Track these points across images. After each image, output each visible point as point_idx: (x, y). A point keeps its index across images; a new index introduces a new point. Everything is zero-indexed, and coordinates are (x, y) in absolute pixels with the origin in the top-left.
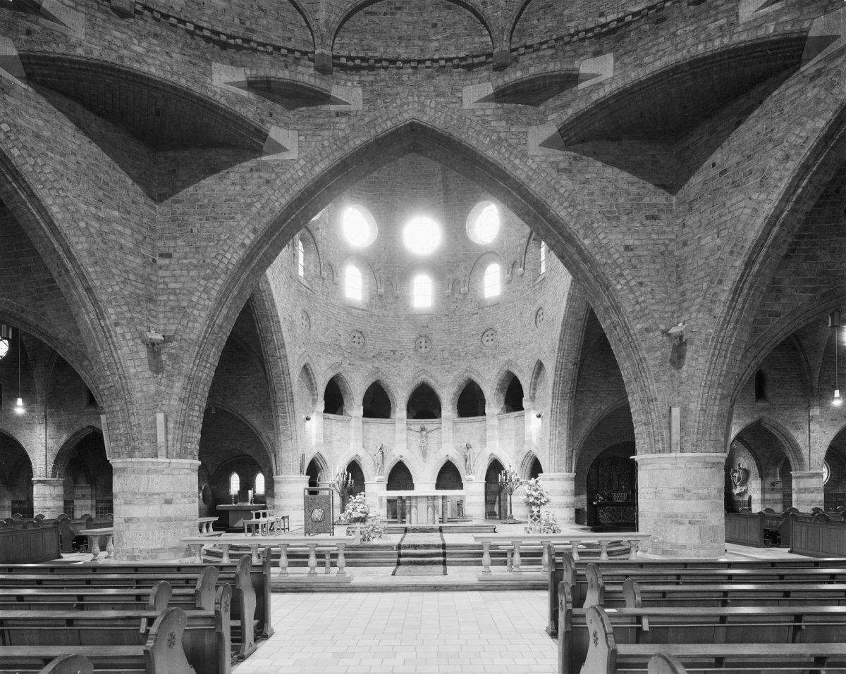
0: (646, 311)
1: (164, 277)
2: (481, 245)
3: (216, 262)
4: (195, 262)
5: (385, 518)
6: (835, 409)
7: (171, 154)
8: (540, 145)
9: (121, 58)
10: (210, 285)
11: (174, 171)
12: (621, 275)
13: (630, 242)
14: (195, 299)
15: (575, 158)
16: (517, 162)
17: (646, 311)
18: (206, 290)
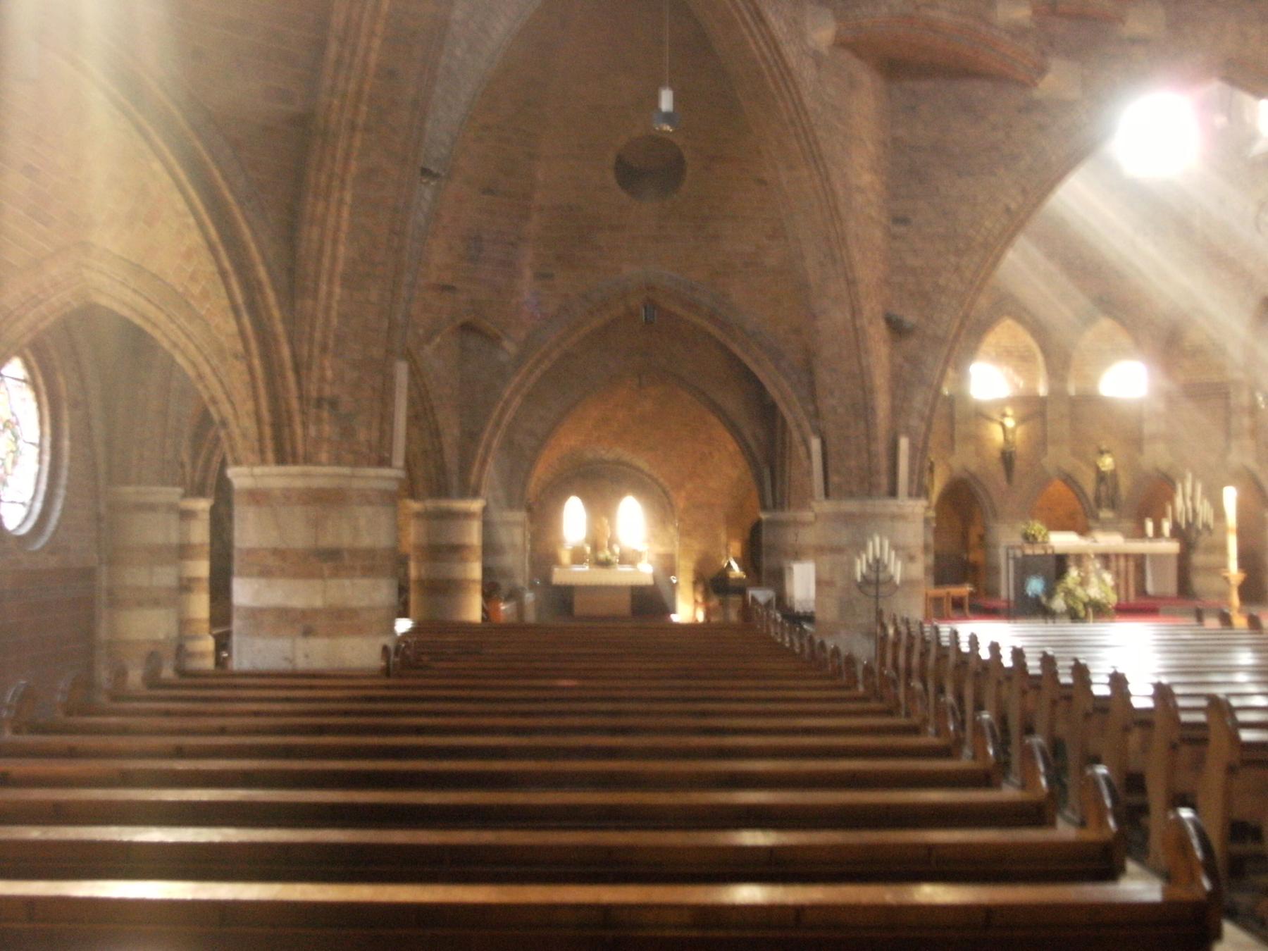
14: (942, 281)
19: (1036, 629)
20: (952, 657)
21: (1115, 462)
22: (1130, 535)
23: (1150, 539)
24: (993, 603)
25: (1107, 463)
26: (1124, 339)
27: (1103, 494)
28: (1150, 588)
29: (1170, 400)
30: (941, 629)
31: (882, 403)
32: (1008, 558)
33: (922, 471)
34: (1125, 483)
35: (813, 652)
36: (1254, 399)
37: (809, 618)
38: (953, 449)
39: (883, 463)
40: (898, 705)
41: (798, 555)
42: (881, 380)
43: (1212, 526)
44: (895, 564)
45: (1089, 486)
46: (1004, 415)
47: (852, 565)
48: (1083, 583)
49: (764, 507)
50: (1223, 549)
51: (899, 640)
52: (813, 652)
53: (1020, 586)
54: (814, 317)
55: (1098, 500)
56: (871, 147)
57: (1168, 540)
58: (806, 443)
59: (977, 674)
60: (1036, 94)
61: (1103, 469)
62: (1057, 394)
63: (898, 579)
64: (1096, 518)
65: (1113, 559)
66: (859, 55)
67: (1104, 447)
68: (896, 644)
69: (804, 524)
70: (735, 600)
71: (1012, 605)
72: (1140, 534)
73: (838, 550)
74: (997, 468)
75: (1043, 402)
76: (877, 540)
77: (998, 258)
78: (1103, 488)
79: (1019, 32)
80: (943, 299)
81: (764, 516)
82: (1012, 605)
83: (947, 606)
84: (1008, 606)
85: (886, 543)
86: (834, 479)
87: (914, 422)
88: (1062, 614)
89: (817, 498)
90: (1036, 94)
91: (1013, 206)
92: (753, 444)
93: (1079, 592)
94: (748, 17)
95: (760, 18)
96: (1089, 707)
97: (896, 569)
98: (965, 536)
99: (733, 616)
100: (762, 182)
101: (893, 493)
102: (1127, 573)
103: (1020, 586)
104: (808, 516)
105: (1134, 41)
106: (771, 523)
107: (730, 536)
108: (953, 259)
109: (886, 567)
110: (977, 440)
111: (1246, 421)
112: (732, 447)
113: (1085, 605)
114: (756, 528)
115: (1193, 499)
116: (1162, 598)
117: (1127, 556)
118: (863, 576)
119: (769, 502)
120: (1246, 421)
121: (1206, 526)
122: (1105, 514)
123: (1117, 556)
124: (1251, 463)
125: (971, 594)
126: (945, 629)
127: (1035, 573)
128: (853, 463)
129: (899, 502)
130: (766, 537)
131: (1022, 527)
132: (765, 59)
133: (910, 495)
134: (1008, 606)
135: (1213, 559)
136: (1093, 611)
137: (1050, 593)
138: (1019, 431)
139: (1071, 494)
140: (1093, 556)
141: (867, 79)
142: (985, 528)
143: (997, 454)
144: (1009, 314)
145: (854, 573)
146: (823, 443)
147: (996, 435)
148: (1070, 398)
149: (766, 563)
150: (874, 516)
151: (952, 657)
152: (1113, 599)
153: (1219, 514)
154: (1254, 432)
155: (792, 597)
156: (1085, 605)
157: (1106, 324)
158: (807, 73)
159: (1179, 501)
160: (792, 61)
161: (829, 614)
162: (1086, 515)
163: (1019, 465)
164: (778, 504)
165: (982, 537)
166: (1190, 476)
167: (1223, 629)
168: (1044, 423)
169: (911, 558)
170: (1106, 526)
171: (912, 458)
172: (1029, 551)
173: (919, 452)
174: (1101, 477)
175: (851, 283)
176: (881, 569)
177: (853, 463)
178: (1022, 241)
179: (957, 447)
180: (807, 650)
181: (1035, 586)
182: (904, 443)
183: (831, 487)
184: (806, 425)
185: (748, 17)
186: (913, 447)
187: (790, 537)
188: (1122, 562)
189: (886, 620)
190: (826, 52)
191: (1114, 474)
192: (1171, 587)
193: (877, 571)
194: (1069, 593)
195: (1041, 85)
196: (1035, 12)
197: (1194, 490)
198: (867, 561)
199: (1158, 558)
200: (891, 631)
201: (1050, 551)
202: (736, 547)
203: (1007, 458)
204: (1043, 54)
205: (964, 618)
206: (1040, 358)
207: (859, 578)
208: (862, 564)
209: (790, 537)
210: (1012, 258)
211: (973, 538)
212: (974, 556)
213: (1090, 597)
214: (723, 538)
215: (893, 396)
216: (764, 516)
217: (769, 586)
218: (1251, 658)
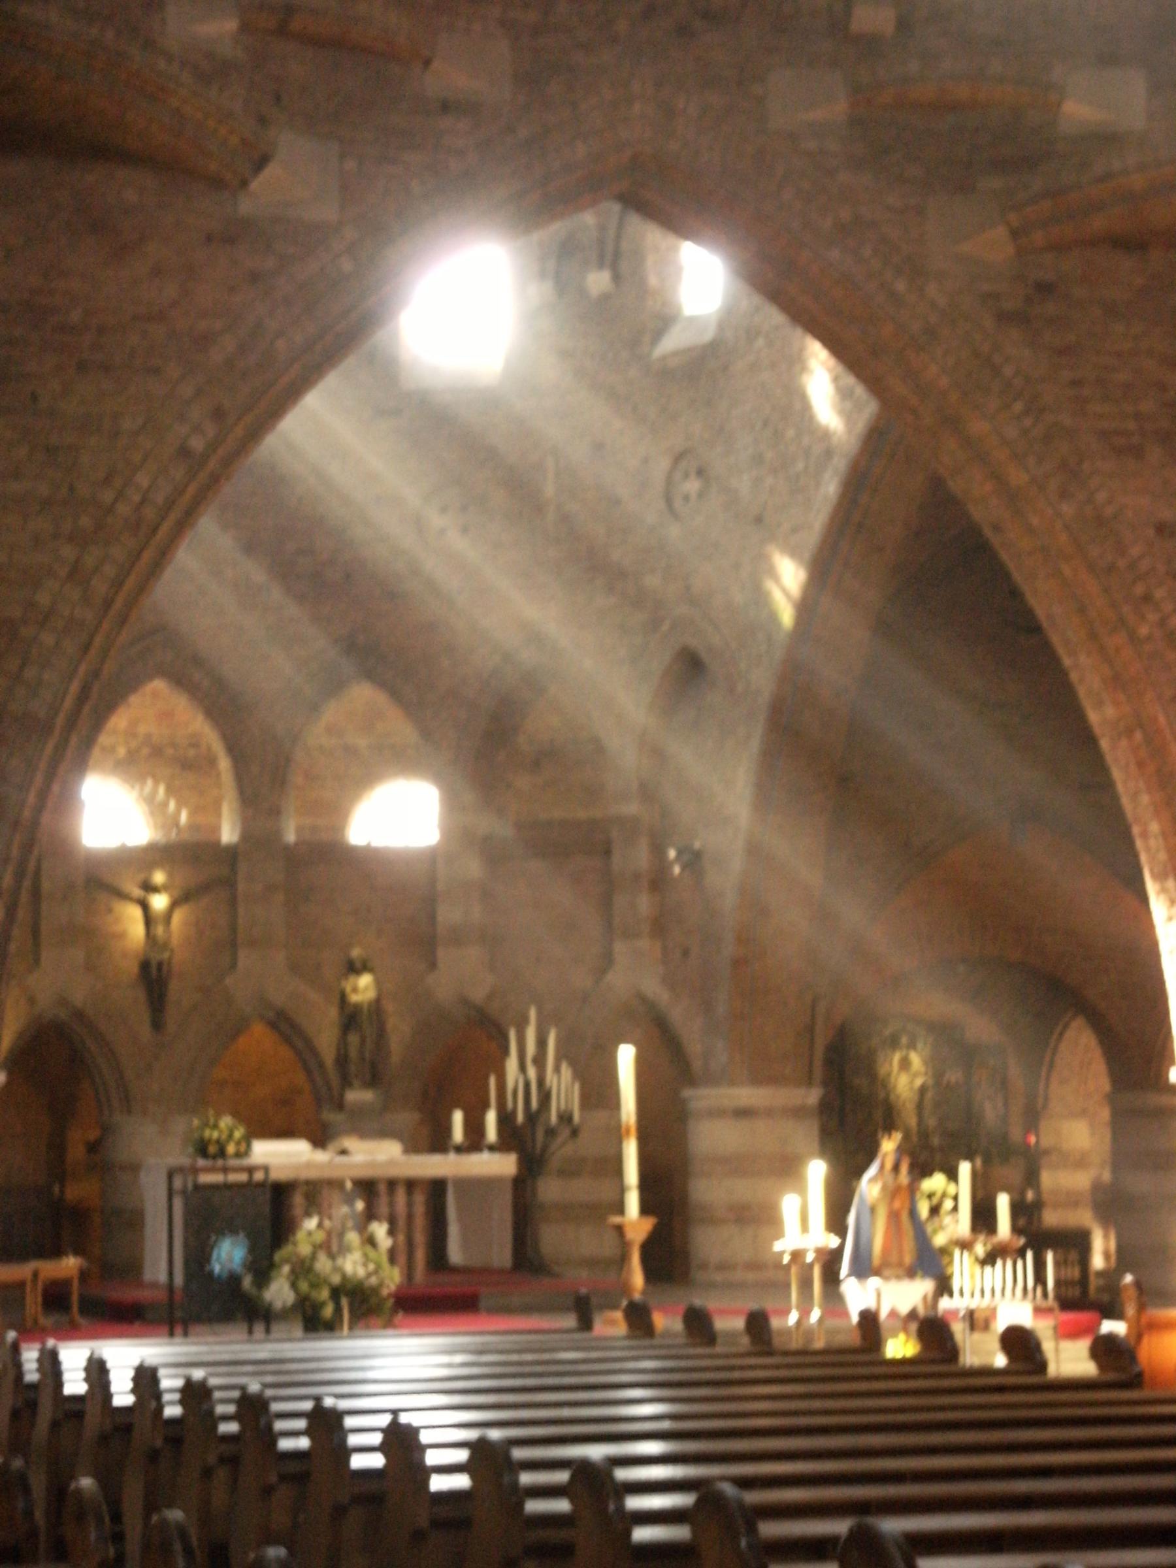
14: (43, 599)
19: (217, 1348)
20: (93, 1420)
21: (378, 982)
23: (459, 1149)
25: (363, 987)
26: (401, 728)
27: (353, 1053)
28: (455, 1254)
38: (37, 961)
40: (33, 1534)
45: (326, 1040)
46: (150, 888)
48: (332, 1246)
50: (618, 1170)
53: (198, 1257)
55: (342, 1060)
59: (153, 1456)
64: (340, 1106)
67: (356, 953)
72: (439, 1142)
74: (134, 1001)
75: (231, 855)
77: (164, 554)
78: (353, 1039)
80: (48, 639)
88: (285, 1315)
90: (245, 206)
91: (197, 444)
93: (323, 1264)
96: (423, 1522)
98: (58, 1147)
102: (410, 1217)
103: (198, 1257)
108: (68, 552)
111: (644, 903)
113: (336, 1293)
115: (539, 1060)
116: (483, 1272)
117: (411, 1184)
120: (644, 903)
121: (566, 1117)
122: (357, 1096)
123: (392, 1184)
124: (653, 987)
125: (84, 1275)
127: (230, 1228)
131: (181, 1125)
135: (581, 1190)
137: (262, 1270)
138: (177, 918)
139: (285, 1052)
140: (349, 1185)
142: (107, 1129)
143: (133, 968)
148: (286, 848)
151: (46, 1413)
152: (392, 1278)
154: (659, 927)
156: (336, 1293)
157: (363, 694)
162: (318, 1101)
163: (179, 993)
165: (93, 1147)
166: (533, 1014)
168: (233, 902)
172: (206, 1178)
174: (351, 1018)
178: (207, 525)
179: (48, 955)
188: (401, 1197)
191: (377, 1006)
192: (502, 1255)
194: (303, 1269)
195: (255, 185)
196: (245, 27)
197: (542, 1043)
201: (259, 1176)
204: (263, 120)
205: (72, 1332)
206: (224, 764)
211: (76, 1152)
212: (74, 1192)
213: (344, 1276)
218: (284, 1302)
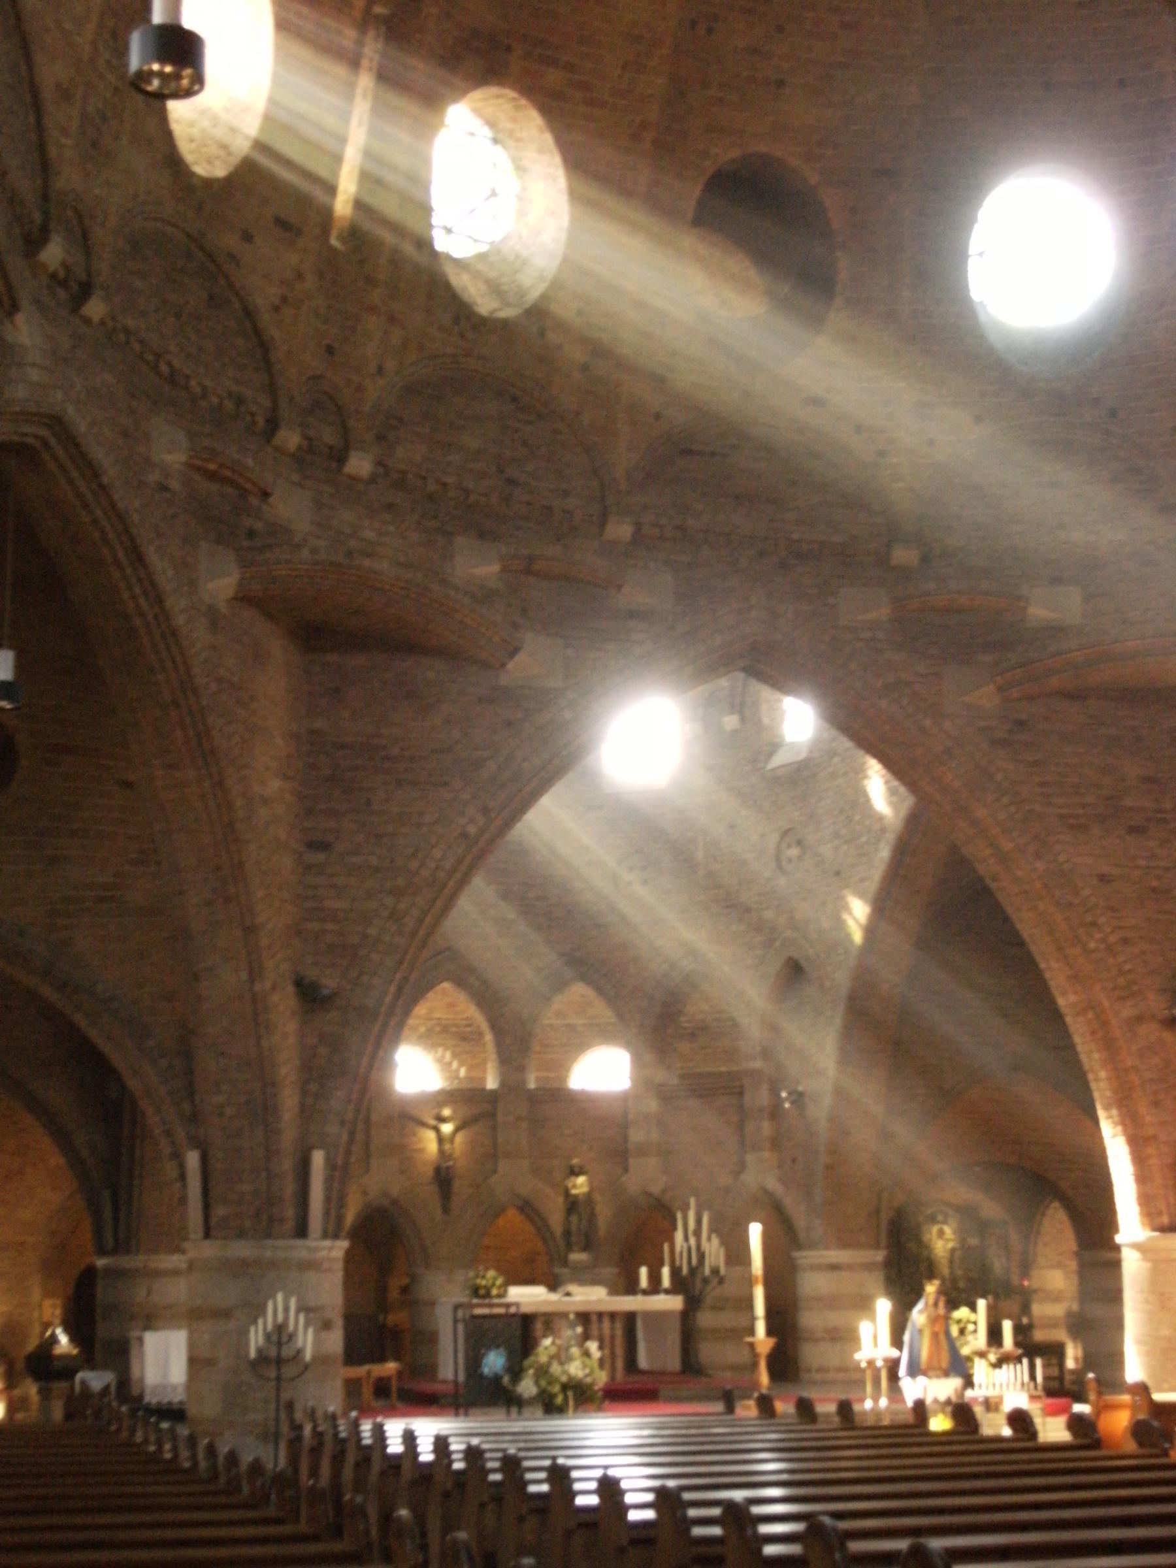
0: (1135, 988)
1: (316, 887)
2: (888, 1300)
3: (414, 865)
4: (374, 861)
5: (795, 1420)
6: (1093, 1372)
7: (332, 658)
8: (954, 849)
9: (350, 554)
10: (402, 906)
11: (337, 690)
12: (1094, 924)
13: (1105, 869)
14: (373, 931)
15: (994, 879)
16: (928, 723)
17: (1135, 988)
18: (395, 916)
20: (407, 1473)
22: (614, 1291)
23: (645, 1292)
24: (437, 1388)
25: (580, 1184)
26: (603, 1012)
27: (574, 1227)
28: (643, 1362)
29: (664, 1094)
30: (386, 1428)
31: (289, 1100)
32: (456, 1321)
33: (335, 1201)
34: (604, 1213)
35: (214, 1467)
36: (777, 1103)
37: (175, 1414)
39: (289, 1188)
41: (150, 1321)
42: (287, 1070)
43: (723, 1271)
44: (305, 1332)
45: (556, 1220)
47: (244, 1333)
48: (561, 1356)
49: (102, 1252)
50: (747, 1304)
51: (321, 1444)
52: (214, 1467)
54: (196, 978)
56: (279, 741)
57: (667, 1292)
58: (178, 1156)
59: (447, 1495)
60: (504, 680)
61: (574, 1192)
62: (511, 1087)
63: (308, 1355)
64: (565, 1263)
65: (594, 1318)
66: (270, 616)
68: (316, 1451)
69: (158, 1273)
70: (60, 1386)
71: (462, 1391)
72: (631, 1288)
73: (224, 1314)
74: (430, 1194)
75: (493, 1097)
76: (280, 1297)
78: (574, 1219)
79: (485, 596)
80: (375, 957)
81: (101, 1262)
82: (462, 1391)
83: (367, 1391)
84: (457, 1390)
85: (293, 1302)
86: (220, 1211)
87: (332, 1129)
88: (531, 1402)
89: (192, 1236)
90: (504, 680)
91: (472, 830)
92: (85, 1153)
93: (556, 1369)
94: (121, 554)
95: (137, 557)
97: (307, 1341)
99: (58, 1412)
100: (128, 785)
101: (302, 1231)
102: (613, 1337)
103: (474, 1363)
104: (175, 1261)
105: (632, 615)
106: (114, 1274)
107: (47, 1294)
108: (389, 901)
109: (292, 1337)
110: (402, 1151)
111: (766, 1128)
112: (57, 1160)
114: (88, 1277)
115: (698, 1233)
117: (613, 1316)
118: (260, 1351)
119: (110, 1242)
120: (766, 1128)
121: (715, 1271)
122: (578, 1257)
123: (600, 1315)
124: (772, 1184)
125: (400, 1374)
126: (394, 1429)
127: (494, 1344)
128: (247, 1187)
129: (310, 1243)
130: (103, 1294)
132: (141, 614)
133: (325, 1235)
134: (457, 1390)
135: (726, 1319)
136: (574, 1396)
137: (516, 1373)
138: (459, 1138)
139: (529, 1227)
141: (278, 647)
142: (414, 1278)
143: (429, 1172)
144: (447, 977)
145: (247, 1345)
146: (204, 1159)
147: (429, 1143)
149: (103, 1330)
150: (273, 1264)
151: (376, 1466)
152: (601, 1378)
153: (738, 1253)
154: (776, 1143)
155: (141, 1380)
156: (565, 1387)
157: (579, 990)
158: (198, 636)
159: (679, 1236)
160: (180, 620)
161: (208, 1408)
163: (457, 1185)
164: (122, 1246)
165: (405, 1290)
166: (692, 1201)
167: (801, 1424)
168: (494, 1128)
169: (327, 1325)
170: (585, 1277)
171: (329, 1180)
172: (479, 1311)
173: (338, 1173)
174: (573, 1205)
175: (250, 930)
176: (285, 1339)
177: (247, 1187)
178: (478, 882)
180: (203, 1464)
181: (494, 1361)
182: (318, 1158)
183: (214, 1221)
184: (181, 1134)
185: (121, 554)
186: (331, 1164)
187: (139, 1293)
188: (606, 1324)
189: (299, 1416)
190: (223, 607)
192: (674, 1362)
193: (280, 1344)
194: (542, 1372)
195: (510, 666)
196: (505, 569)
197: (699, 1221)
198: (265, 1328)
199: (656, 1318)
200: (307, 1430)
202: (52, 1309)
203: (443, 1177)
204: (516, 626)
205: (393, 1412)
206: (489, 1037)
207: (253, 1354)
208: (256, 1332)
209: (139, 1293)
210: (464, 904)
211: (394, 1294)
212: (395, 1318)
213: (569, 1376)
214: (36, 1294)
215: (304, 1093)
216: (101, 1262)
217: (105, 1367)
